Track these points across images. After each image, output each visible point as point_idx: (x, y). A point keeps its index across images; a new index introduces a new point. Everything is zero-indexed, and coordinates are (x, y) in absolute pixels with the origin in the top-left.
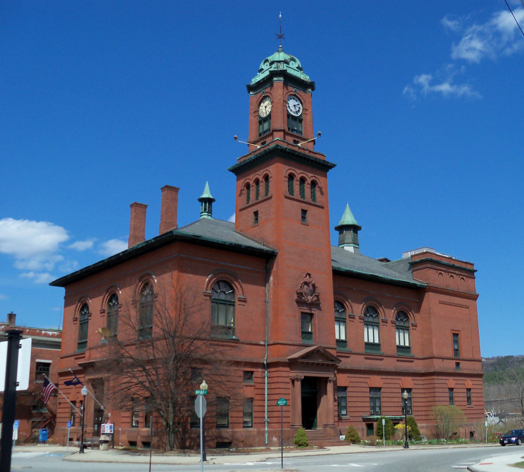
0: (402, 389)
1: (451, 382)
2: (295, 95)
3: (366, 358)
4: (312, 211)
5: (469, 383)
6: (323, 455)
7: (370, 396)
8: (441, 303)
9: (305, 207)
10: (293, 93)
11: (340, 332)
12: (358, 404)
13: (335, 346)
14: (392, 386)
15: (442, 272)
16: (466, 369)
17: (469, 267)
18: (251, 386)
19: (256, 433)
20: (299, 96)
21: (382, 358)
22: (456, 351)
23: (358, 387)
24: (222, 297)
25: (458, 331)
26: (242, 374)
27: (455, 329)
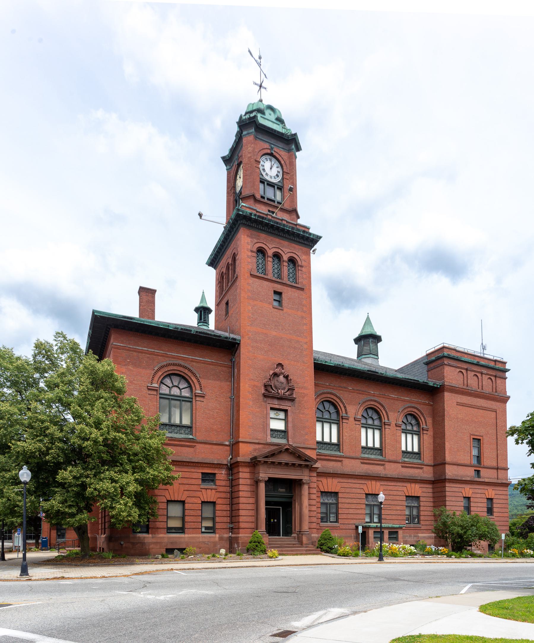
0: (366, 494)
1: (468, 490)
2: (271, 155)
3: (362, 463)
4: (288, 293)
5: (491, 492)
6: (247, 567)
7: (406, 504)
8: (458, 404)
9: (279, 288)
10: (269, 151)
11: (326, 433)
12: (351, 511)
13: (314, 447)
14: (395, 493)
15: (462, 370)
16: (487, 478)
17: (499, 366)
18: (211, 489)
19: (217, 539)
20: (277, 156)
21: (383, 463)
22: (479, 458)
23: (351, 495)
24: (175, 391)
25: (480, 436)
26: (200, 476)
27: (476, 434)
